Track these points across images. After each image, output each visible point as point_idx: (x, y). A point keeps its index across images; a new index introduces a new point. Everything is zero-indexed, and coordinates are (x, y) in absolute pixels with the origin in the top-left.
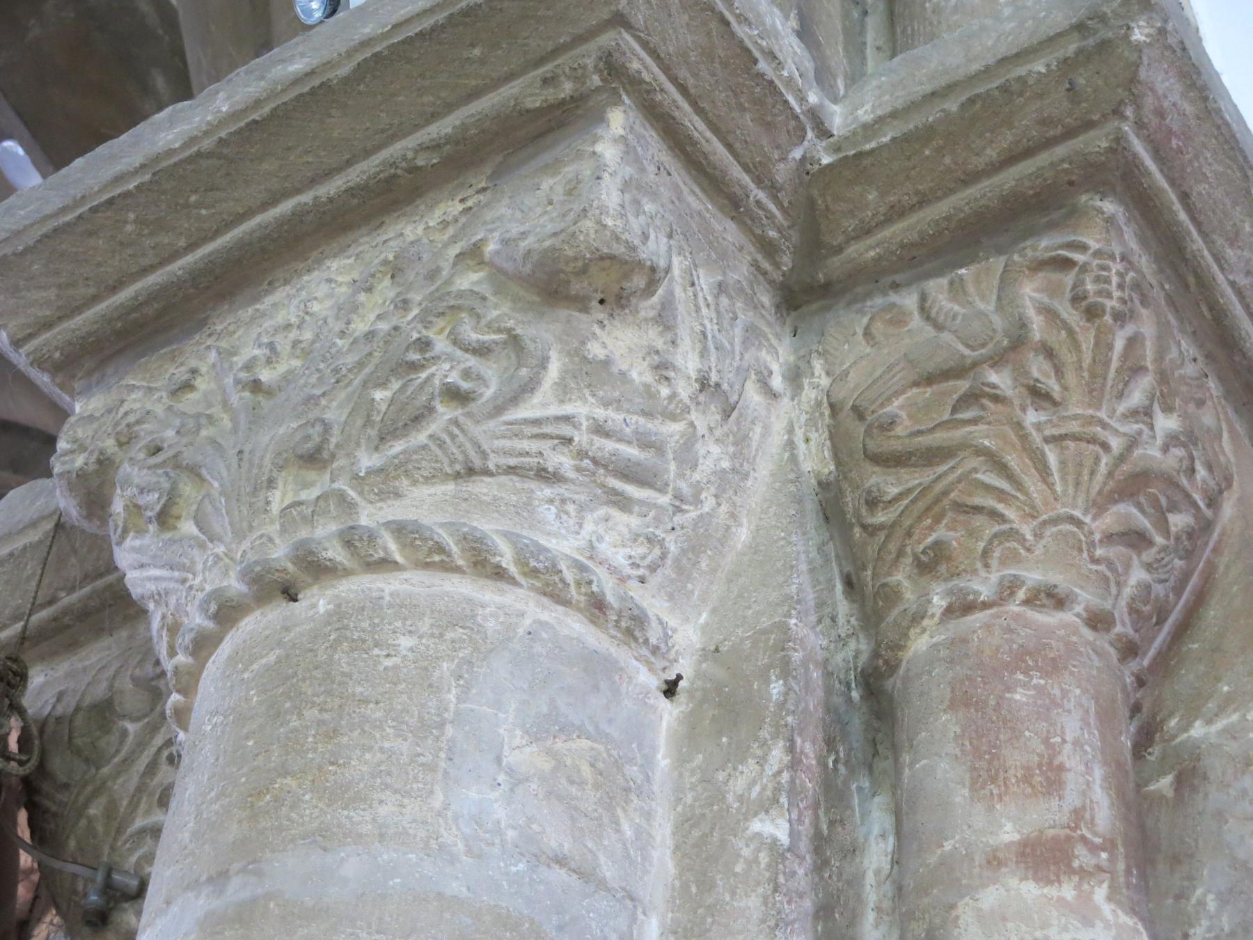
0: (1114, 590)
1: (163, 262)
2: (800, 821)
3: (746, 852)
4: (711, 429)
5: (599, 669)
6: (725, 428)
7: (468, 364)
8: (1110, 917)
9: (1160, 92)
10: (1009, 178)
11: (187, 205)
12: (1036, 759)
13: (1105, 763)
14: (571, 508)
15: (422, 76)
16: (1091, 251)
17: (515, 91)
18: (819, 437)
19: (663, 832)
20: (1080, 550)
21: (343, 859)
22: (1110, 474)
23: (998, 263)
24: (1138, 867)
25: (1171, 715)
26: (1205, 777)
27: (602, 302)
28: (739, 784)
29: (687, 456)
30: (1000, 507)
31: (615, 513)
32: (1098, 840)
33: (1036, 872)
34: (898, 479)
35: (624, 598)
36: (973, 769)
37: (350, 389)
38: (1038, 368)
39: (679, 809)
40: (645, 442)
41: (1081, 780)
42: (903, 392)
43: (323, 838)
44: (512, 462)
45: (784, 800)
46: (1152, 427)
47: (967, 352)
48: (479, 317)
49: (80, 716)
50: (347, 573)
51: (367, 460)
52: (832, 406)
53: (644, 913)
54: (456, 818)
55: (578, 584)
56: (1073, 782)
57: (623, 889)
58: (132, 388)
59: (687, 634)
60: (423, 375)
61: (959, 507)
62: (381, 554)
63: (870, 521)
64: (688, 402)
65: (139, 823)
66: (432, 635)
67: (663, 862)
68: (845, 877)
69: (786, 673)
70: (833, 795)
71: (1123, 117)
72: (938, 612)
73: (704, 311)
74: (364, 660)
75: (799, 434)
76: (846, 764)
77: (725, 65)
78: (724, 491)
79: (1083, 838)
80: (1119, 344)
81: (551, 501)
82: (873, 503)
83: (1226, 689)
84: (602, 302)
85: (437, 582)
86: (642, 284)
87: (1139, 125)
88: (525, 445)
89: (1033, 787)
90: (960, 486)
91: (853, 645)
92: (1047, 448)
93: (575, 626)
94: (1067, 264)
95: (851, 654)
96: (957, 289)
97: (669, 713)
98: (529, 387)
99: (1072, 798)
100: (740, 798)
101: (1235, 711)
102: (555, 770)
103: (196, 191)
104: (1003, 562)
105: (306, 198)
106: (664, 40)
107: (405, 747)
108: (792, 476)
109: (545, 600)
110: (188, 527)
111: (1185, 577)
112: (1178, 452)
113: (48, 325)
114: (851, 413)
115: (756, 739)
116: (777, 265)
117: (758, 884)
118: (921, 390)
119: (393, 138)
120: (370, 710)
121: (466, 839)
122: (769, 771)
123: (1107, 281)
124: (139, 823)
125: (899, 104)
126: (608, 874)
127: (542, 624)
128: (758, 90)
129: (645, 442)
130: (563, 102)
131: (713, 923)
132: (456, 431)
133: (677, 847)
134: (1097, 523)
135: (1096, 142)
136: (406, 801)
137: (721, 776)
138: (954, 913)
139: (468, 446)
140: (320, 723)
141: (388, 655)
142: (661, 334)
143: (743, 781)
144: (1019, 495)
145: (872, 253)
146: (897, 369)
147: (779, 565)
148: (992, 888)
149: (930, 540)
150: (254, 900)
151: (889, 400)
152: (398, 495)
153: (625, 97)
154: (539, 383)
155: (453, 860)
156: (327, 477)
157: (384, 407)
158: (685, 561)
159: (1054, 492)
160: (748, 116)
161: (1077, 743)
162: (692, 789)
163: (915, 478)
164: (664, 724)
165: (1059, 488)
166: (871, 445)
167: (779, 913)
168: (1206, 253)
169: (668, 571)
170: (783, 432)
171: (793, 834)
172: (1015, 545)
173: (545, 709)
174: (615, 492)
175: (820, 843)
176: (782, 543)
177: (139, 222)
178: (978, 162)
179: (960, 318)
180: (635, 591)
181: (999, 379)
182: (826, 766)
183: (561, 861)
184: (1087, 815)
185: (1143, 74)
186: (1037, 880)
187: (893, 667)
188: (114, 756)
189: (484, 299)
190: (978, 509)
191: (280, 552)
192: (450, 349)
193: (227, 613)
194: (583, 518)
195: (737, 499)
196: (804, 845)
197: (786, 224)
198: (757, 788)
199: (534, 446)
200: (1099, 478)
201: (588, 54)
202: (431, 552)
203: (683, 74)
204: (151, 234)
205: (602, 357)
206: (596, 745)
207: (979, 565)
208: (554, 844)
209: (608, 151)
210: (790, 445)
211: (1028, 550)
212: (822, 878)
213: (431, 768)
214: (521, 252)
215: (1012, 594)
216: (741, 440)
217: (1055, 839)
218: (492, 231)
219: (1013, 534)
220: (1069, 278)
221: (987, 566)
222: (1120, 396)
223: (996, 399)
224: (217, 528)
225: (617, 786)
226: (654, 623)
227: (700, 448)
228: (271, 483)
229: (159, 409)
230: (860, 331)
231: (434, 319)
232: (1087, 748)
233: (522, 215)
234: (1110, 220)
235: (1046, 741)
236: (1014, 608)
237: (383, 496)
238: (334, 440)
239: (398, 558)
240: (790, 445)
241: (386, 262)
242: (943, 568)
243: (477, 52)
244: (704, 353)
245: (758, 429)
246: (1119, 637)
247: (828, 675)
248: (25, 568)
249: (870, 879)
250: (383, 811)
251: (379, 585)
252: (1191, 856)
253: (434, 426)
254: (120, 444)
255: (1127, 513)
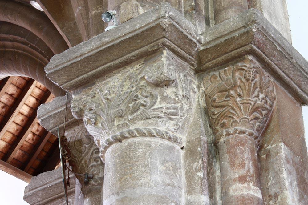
0: (253, 128)
2: (205, 172)
3: (197, 179)
4: (185, 103)
5: (171, 149)
6: (188, 102)
7: (145, 100)
8: (253, 188)
9: (258, 38)
10: (233, 53)
11: (90, 64)
12: (241, 162)
13: (252, 161)
14: (164, 122)
15: (130, 44)
16: (247, 67)
17: (147, 48)
18: (203, 99)
19: (183, 174)
20: (247, 123)
21: (137, 190)
22: (252, 109)
23: (232, 67)
24: (258, 177)
25: (265, 144)
26: (271, 156)
27: (165, 86)
28: (195, 166)
29: (182, 109)
30: (233, 116)
31: (171, 121)
32: (251, 175)
33: (241, 182)
34: (217, 110)
35: (174, 136)
36: (231, 164)
37: (125, 103)
38: (239, 90)
39: (186, 170)
40: (174, 108)
41: (248, 165)
42: (217, 94)
43: (133, 186)
44: (154, 116)
45: (202, 170)
46: (259, 98)
47: (227, 87)
48: (145, 90)
49: (76, 142)
50: (129, 138)
51: (130, 117)
52: (205, 95)
53: (182, 189)
54: (152, 181)
55: (166, 136)
56: (246, 165)
57: (178, 186)
58: (84, 95)
59: (184, 138)
60: (137, 102)
61: (227, 116)
62: (135, 135)
63: (212, 117)
64: (181, 100)
65: (91, 164)
66: (145, 149)
67: (184, 180)
68: (213, 178)
69: (201, 147)
70: (210, 164)
71: (252, 44)
72: (225, 135)
73: (182, 82)
74: (135, 154)
75: (200, 98)
76: (212, 158)
77: (182, 39)
78: (188, 113)
79: (248, 175)
80: (252, 85)
81: (161, 121)
82: (213, 114)
83: (274, 139)
84: (165, 86)
85: (144, 139)
86: (172, 83)
87: (255, 45)
88: (155, 113)
89: (240, 167)
90: (227, 113)
91: (211, 136)
92: (241, 105)
93: (167, 142)
94: (243, 70)
95: (211, 138)
96: (225, 72)
97: (182, 152)
98: (155, 103)
99: (246, 168)
100: (195, 169)
101: (276, 143)
102: (166, 169)
103: (91, 61)
104: (235, 126)
105: (112, 63)
106: (172, 38)
107: (143, 169)
108: (199, 108)
109: (161, 139)
110: (100, 125)
111: (266, 120)
112: (264, 101)
113: (66, 82)
114: (208, 97)
115: (197, 159)
116: (194, 67)
117: (199, 184)
118: (220, 93)
119: (126, 55)
120: (136, 163)
121: (154, 184)
122: (199, 164)
123: (250, 74)
124: (91, 164)
125: (213, 38)
126: (176, 185)
127: (162, 143)
128: (188, 41)
129: (174, 108)
130: (155, 50)
131: (193, 191)
132: (144, 112)
133: (186, 177)
134: (250, 117)
135: (247, 48)
136: (144, 179)
137: (192, 165)
138: (229, 189)
139: (146, 114)
140: (129, 166)
141: (138, 153)
142: (176, 89)
143: (196, 166)
144: (236, 114)
145: (210, 65)
146: (216, 89)
147: (198, 125)
148: (234, 185)
149: (223, 121)
150: (124, 197)
151: (214, 95)
152: (136, 123)
153: (166, 48)
154: (157, 102)
155: (153, 188)
156: (123, 119)
157: (131, 107)
158: (183, 126)
159: (242, 113)
160: (187, 46)
161: (247, 158)
162: (187, 166)
163: (220, 110)
164: (182, 154)
165: (243, 113)
166: (212, 105)
167: (202, 189)
168: (269, 60)
169: (180, 129)
170: (197, 98)
171: (204, 175)
172: (236, 123)
173: (163, 159)
174: (171, 118)
175: (208, 174)
176: (198, 121)
177: (82, 66)
178: (228, 51)
179: (226, 79)
180: (175, 134)
181: (232, 92)
182: (208, 160)
183: (169, 185)
184: (249, 171)
185: (255, 36)
186: (241, 184)
187: (218, 142)
188: (84, 152)
189: (146, 87)
190: (230, 117)
191: (118, 133)
192: (141, 97)
193: (110, 144)
194: (166, 123)
195: (190, 113)
196: (206, 176)
197: (195, 60)
198: (198, 167)
199: (157, 113)
200: (250, 110)
201: (160, 42)
202: (142, 134)
203: (175, 42)
204: (84, 68)
205: (166, 95)
206: (172, 163)
207: (231, 126)
208: (167, 182)
209: (164, 59)
210: (199, 101)
211: (238, 124)
212: (209, 180)
213: (147, 173)
214: (152, 80)
215: (236, 132)
216: (190, 103)
217: (244, 176)
218: (146, 74)
219: (236, 121)
220: (244, 72)
221: (232, 127)
222: (253, 94)
223: (232, 97)
224: (106, 127)
225: (175, 169)
226: (179, 139)
227: (184, 107)
228: (114, 120)
229: (90, 101)
230: (209, 79)
231: (138, 91)
232: (249, 159)
233: (150, 72)
234: (251, 61)
235: (242, 159)
236: (236, 134)
237: (133, 123)
238: (124, 113)
239: (138, 135)
240: (199, 101)
241: (127, 77)
242: (225, 127)
243: (140, 41)
244: (183, 91)
245: (193, 99)
246: (254, 136)
247: (208, 144)
248: (61, 115)
249: (217, 177)
250: (141, 181)
251: (135, 140)
252: (268, 170)
253: (140, 111)
254: (83, 106)
255: (256, 114)
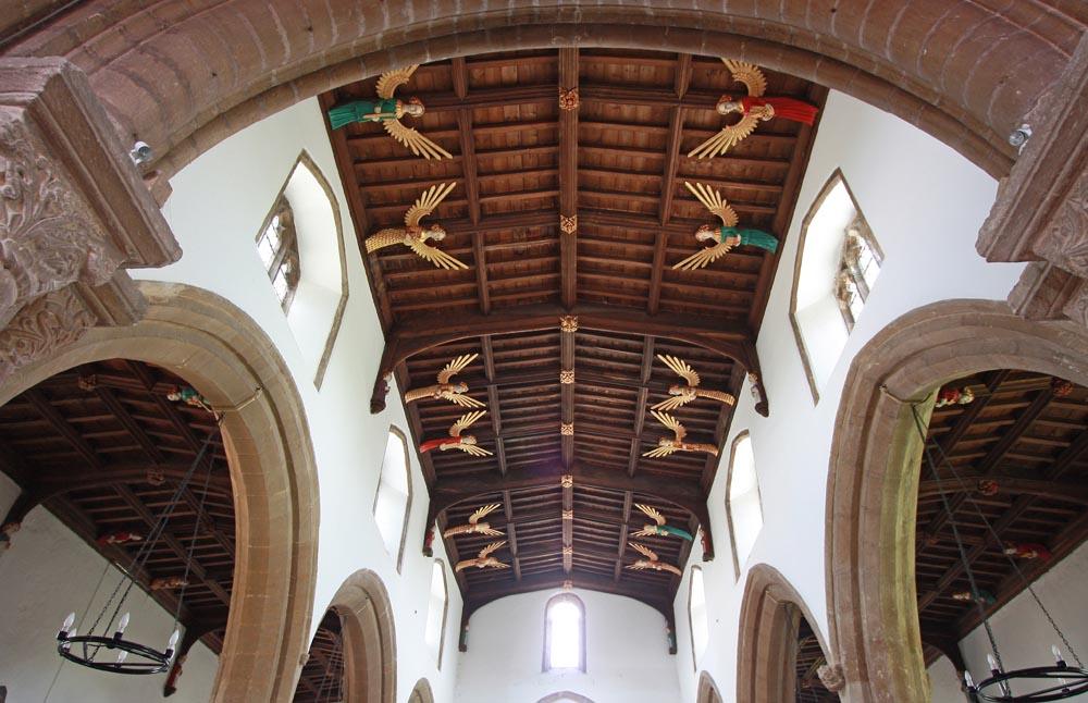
1: (74, 147)
105: (98, 192)
119: (117, 215)
